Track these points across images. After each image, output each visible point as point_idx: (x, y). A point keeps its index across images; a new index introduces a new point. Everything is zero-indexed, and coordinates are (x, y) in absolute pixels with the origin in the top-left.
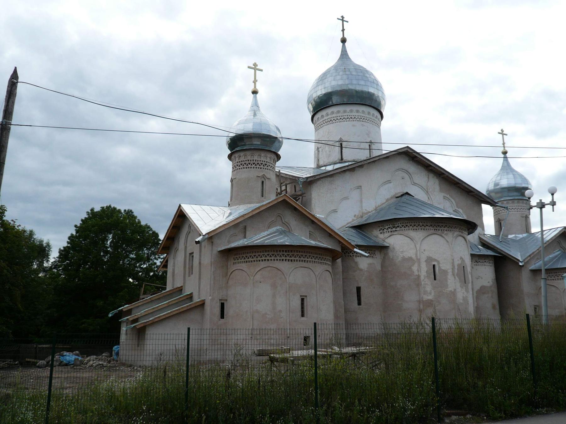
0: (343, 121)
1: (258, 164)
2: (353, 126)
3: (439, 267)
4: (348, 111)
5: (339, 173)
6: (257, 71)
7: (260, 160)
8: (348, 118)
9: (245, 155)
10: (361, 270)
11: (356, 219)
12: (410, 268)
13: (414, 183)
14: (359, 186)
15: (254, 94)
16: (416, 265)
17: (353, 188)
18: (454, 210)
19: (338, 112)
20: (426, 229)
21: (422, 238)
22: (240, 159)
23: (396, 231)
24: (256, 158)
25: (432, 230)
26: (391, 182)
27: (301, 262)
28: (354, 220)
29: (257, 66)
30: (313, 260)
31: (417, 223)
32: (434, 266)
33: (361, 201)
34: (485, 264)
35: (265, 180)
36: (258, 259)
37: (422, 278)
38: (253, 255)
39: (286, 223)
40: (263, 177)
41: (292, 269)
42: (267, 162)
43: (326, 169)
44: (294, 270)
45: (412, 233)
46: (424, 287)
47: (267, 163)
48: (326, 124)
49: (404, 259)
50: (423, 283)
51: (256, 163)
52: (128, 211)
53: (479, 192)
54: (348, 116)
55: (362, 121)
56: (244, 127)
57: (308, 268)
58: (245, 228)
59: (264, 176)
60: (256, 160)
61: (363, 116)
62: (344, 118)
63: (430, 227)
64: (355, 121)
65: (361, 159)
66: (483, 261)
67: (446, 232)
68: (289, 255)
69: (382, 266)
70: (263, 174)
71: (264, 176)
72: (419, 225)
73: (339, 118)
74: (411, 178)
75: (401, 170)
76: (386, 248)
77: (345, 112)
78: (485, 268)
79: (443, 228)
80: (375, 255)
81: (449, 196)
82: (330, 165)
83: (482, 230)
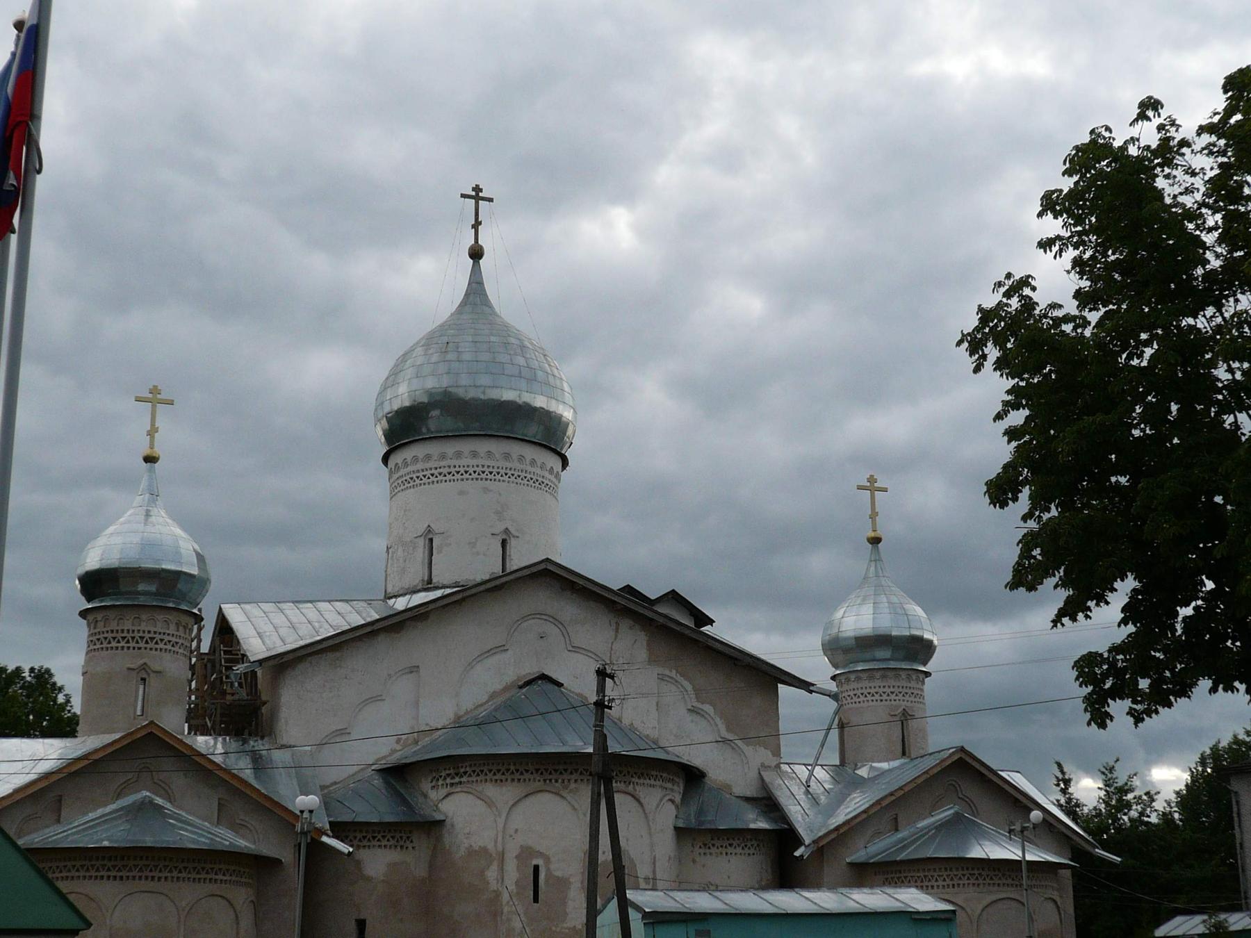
0: (437, 482)
1: (133, 638)
2: (461, 493)
3: (548, 870)
4: (515, 456)
5: (360, 638)
6: (480, 202)
7: (139, 628)
8: (449, 473)
9: (106, 620)
10: (369, 879)
11: (401, 748)
12: (482, 873)
13: (573, 647)
14: (415, 666)
15: (148, 464)
16: (494, 867)
17: (396, 673)
18: (689, 708)
19: (428, 457)
20: (525, 780)
21: (511, 803)
22: (107, 626)
23: (461, 783)
24: (127, 625)
25: (539, 781)
26: (507, 650)
27: (143, 881)
28: (393, 751)
29: (482, 192)
30: (175, 874)
31: (503, 764)
32: (536, 868)
33: (417, 703)
34: (730, 850)
35: (149, 675)
36: (144, 875)
37: (505, 897)
38: (478, 770)
39: (161, 783)
40: (144, 669)
41: (120, 897)
42: (155, 633)
43: (394, 607)
44: (126, 898)
45: (491, 790)
46: (509, 920)
47: (155, 636)
48: (418, 481)
49: (472, 853)
50: (506, 909)
51: (129, 636)
52: (39, 671)
53: (759, 659)
54: (449, 467)
55: (486, 479)
56: (102, 555)
57: (157, 893)
58: (60, 800)
59: (144, 667)
60: (128, 631)
61: (489, 467)
62: (440, 474)
63: (535, 775)
64: (467, 479)
65: (474, 580)
66: (726, 843)
67: (573, 785)
68: (116, 866)
69: (432, 866)
70: (142, 662)
71: (144, 667)
72: (508, 770)
73: (428, 473)
74: (565, 634)
75: (538, 616)
76: (440, 823)
77: (443, 457)
78: (729, 861)
79: (566, 776)
80: (412, 842)
81: (677, 672)
82: (403, 595)
83: (771, 756)
